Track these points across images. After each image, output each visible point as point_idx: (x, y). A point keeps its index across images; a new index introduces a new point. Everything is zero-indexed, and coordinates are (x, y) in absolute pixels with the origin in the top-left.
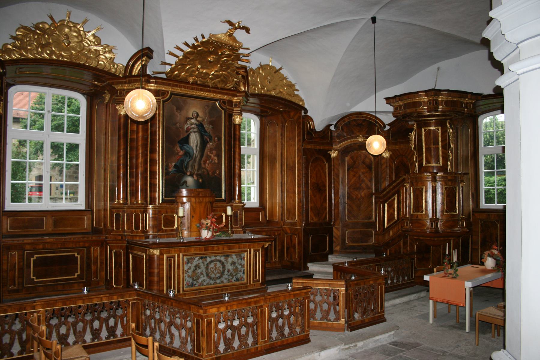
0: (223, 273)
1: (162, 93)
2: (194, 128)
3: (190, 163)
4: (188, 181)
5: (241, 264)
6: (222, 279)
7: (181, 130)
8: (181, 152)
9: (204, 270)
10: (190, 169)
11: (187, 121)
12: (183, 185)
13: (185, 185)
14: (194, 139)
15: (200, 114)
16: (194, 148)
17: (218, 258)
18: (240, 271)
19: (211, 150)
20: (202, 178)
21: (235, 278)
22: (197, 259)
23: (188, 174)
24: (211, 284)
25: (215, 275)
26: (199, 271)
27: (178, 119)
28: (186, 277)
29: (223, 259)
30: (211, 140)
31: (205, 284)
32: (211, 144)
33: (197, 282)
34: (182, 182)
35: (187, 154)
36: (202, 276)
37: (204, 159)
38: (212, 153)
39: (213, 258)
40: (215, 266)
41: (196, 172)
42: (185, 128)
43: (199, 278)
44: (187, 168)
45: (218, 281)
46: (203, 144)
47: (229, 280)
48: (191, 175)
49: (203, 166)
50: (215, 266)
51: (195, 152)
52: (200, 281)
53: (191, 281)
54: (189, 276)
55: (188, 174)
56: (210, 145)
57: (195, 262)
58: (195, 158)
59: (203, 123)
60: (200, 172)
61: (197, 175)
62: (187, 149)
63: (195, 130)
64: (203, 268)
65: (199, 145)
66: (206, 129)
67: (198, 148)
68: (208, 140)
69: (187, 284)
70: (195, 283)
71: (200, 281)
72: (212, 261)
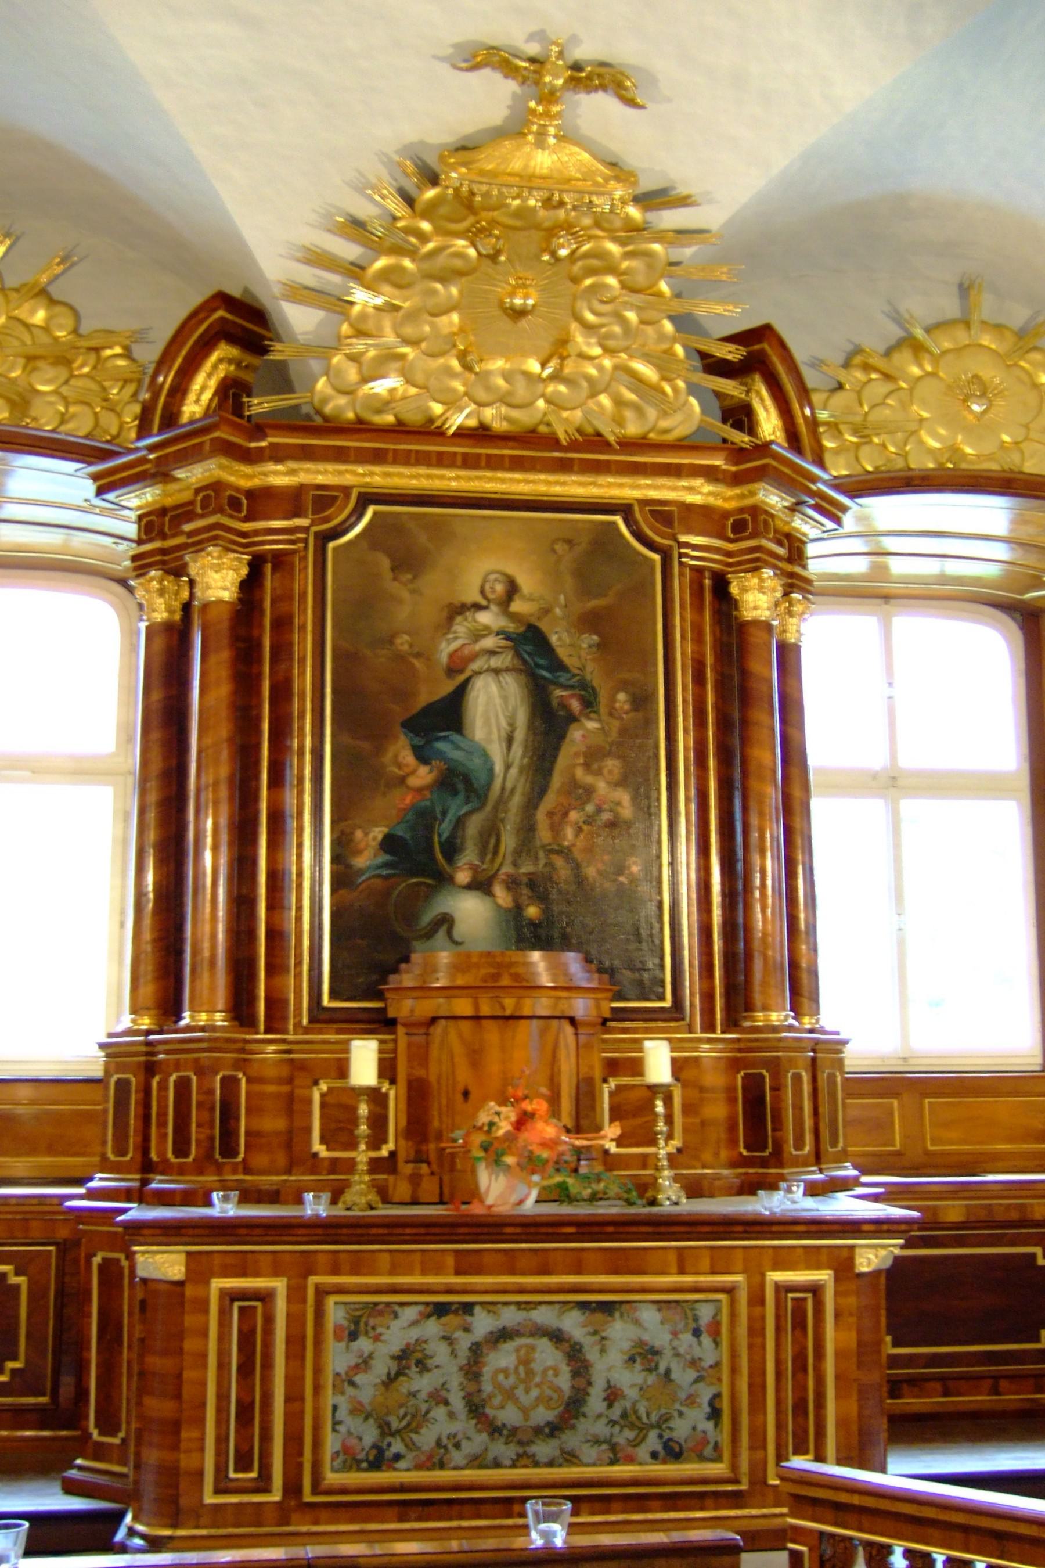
0: (574, 1407)
1: (317, 499)
2: (492, 653)
3: (474, 826)
4: (458, 916)
5: (694, 1363)
6: (571, 1440)
7: (416, 663)
8: (423, 770)
9: (455, 1380)
10: (469, 856)
11: (450, 619)
12: (429, 934)
13: (442, 933)
14: (495, 709)
15: (526, 583)
16: (496, 753)
17: (543, 1316)
18: (691, 1400)
19: (592, 757)
20: (542, 898)
21: (653, 1442)
22: (410, 1314)
23: (463, 877)
24: (497, 1464)
25: (525, 1412)
26: (423, 1384)
27: (402, 614)
28: (342, 1414)
29: (573, 1324)
30: (589, 703)
31: (457, 1457)
32: (592, 725)
33: (411, 1446)
34: (427, 918)
35: (460, 783)
36: (439, 1413)
37: (550, 801)
38: (599, 773)
39: (510, 1317)
40: (526, 1362)
41: (507, 869)
42: (444, 658)
43: (417, 1421)
44: (452, 850)
45: (543, 1449)
46: (549, 724)
47: (614, 1447)
48: (481, 885)
49: (544, 834)
50: (526, 1362)
51: (499, 768)
52: (426, 1438)
53: (370, 1435)
54: (357, 1409)
55: (463, 877)
56: (584, 732)
57: (397, 1334)
58: (502, 801)
59: (544, 626)
60: (526, 868)
61: (512, 884)
62: (456, 755)
63: (495, 662)
64: (446, 1368)
65: (520, 735)
66: (562, 653)
67: (517, 750)
68: (575, 705)
69: (346, 1450)
70: (397, 1446)
71: (426, 1438)
72: (503, 1335)
